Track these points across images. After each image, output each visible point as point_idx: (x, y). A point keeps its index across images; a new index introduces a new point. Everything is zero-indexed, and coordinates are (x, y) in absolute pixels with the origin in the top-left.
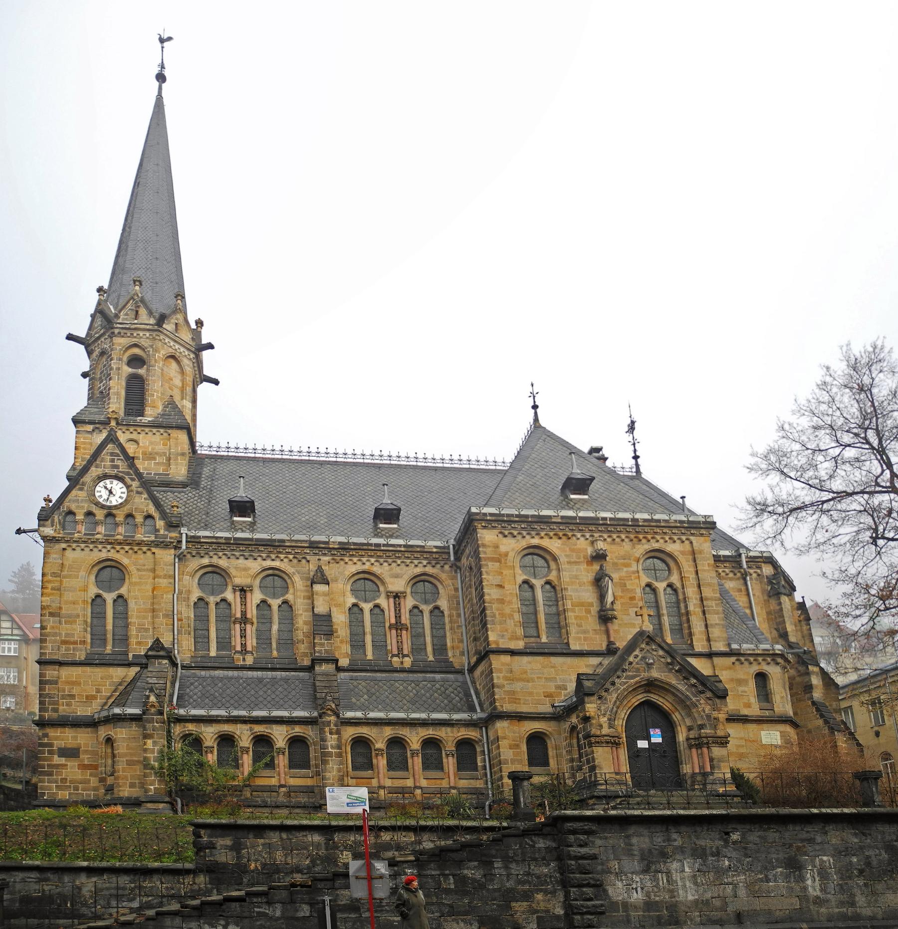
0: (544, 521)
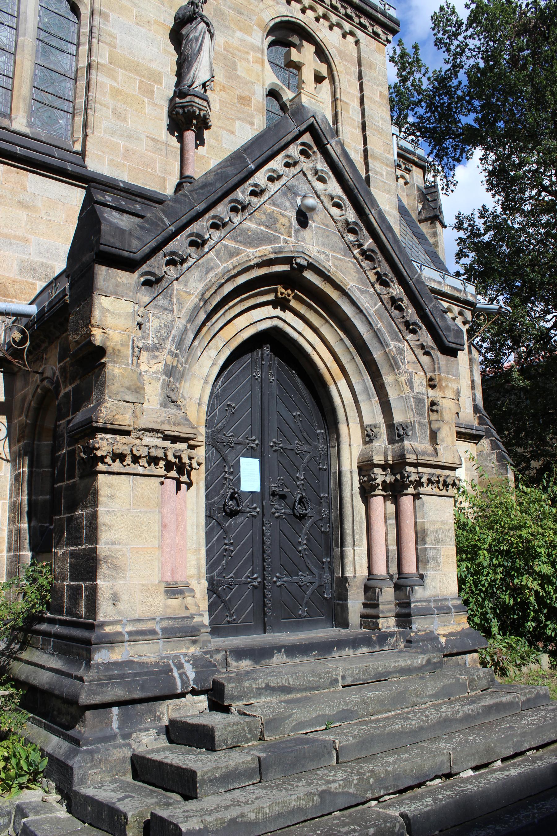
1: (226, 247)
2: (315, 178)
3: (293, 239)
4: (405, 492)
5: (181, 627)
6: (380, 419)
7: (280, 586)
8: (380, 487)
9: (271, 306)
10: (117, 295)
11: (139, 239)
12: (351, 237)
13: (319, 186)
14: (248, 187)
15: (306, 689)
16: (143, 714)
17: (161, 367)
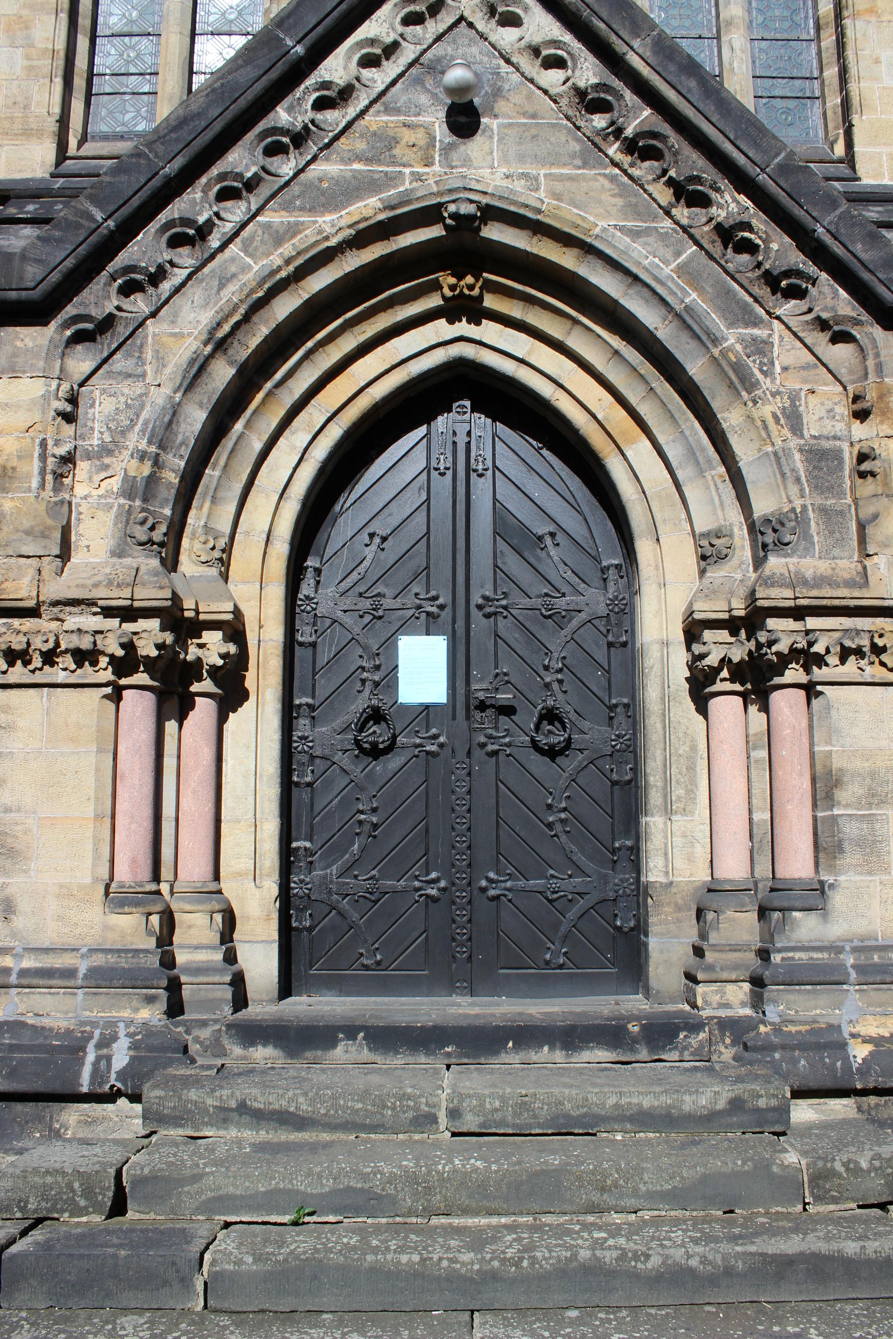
1: (268, 226)
2: (493, 22)
3: (437, 168)
4: (777, 680)
5: (130, 969)
6: (734, 516)
7: (497, 898)
8: (725, 674)
9: (443, 320)
10: (14, 371)
11: (39, 261)
12: (599, 121)
13: (507, 37)
14: (306, 92)
15: (346, 1126)
16: (27, 1122)
17: (115, 484)
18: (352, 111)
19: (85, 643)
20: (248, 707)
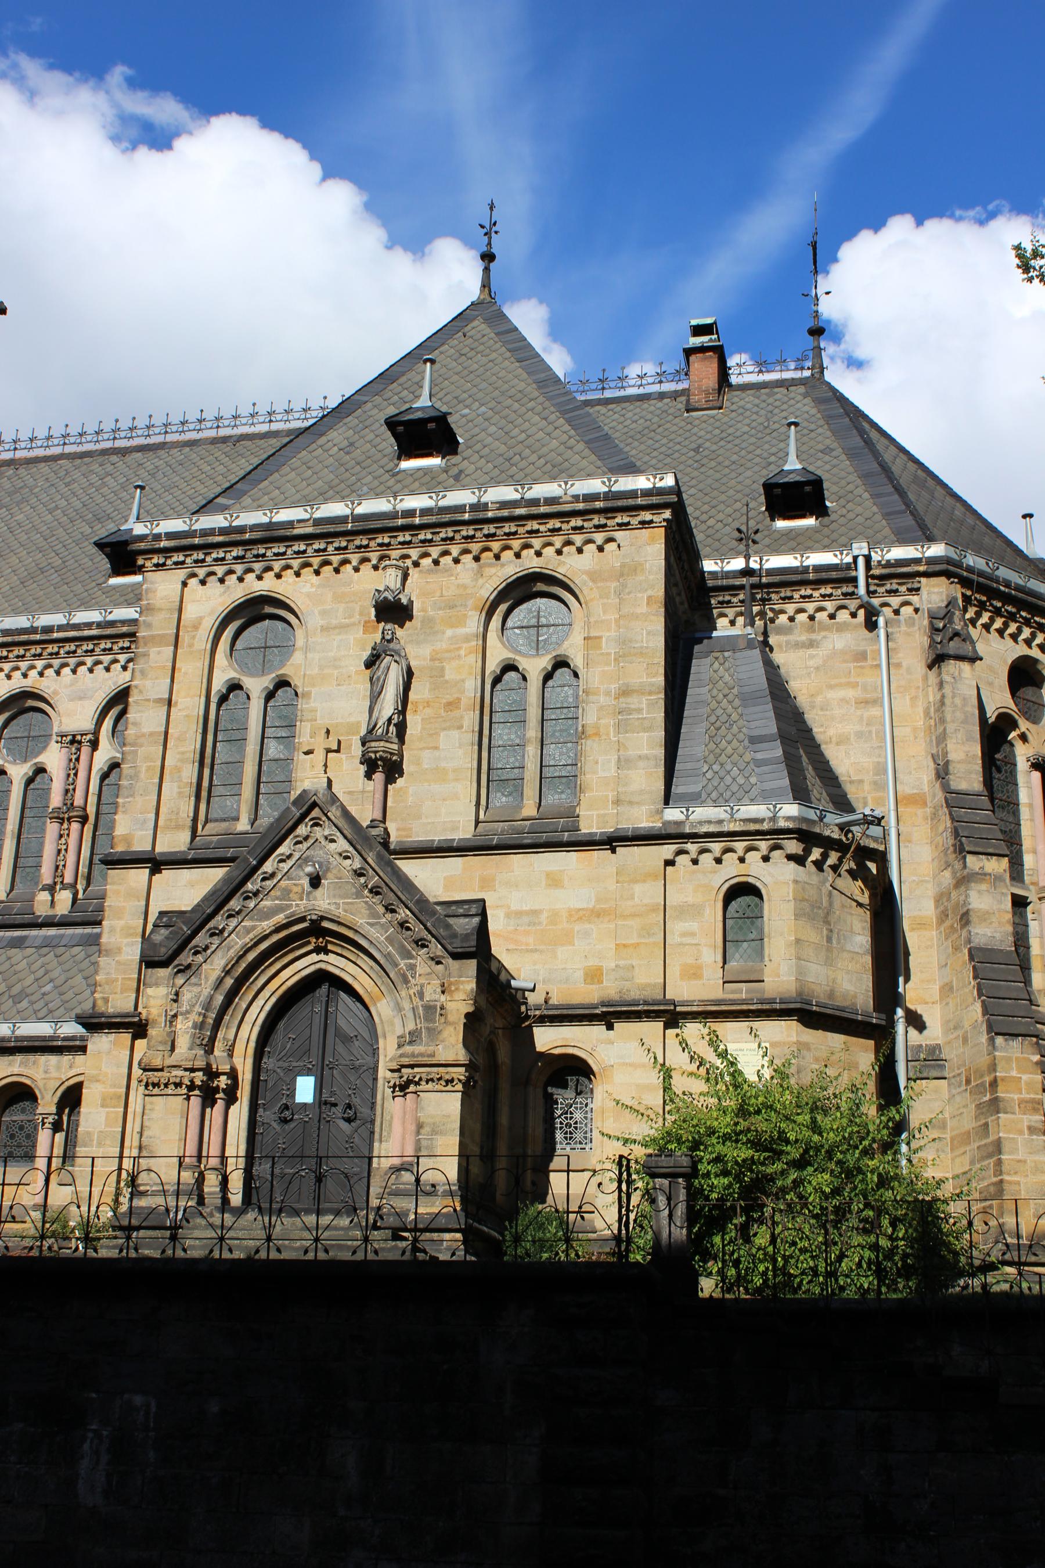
0: (274, 535)
14: (258, 876)
17: (190, 1024)
18: (275, 881)
19: (178, 1080)
20: (238, 1103)
